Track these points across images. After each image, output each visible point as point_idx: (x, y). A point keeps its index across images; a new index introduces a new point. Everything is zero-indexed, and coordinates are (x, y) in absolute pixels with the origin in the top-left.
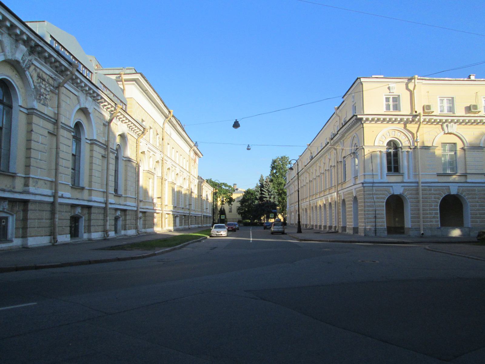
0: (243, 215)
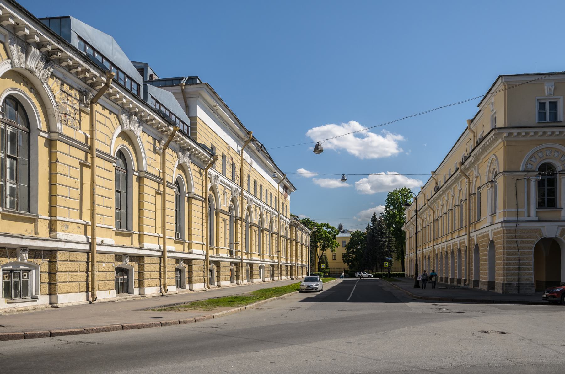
0: (350, 264)
